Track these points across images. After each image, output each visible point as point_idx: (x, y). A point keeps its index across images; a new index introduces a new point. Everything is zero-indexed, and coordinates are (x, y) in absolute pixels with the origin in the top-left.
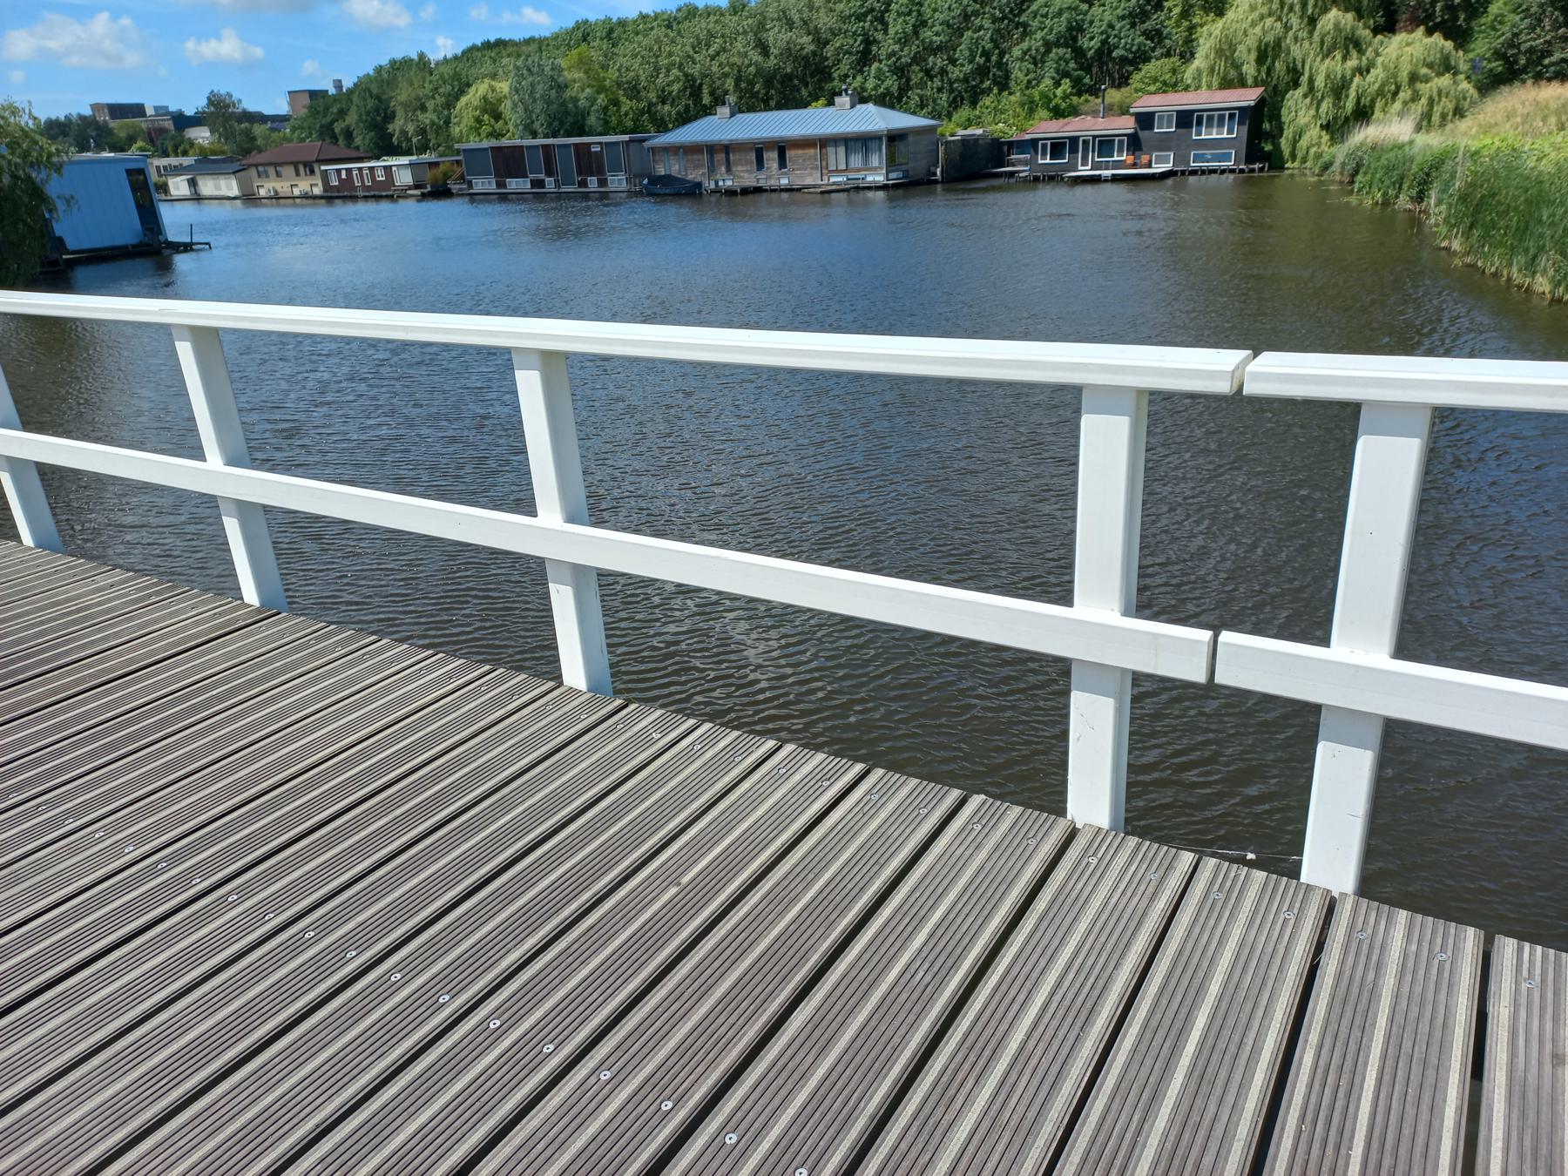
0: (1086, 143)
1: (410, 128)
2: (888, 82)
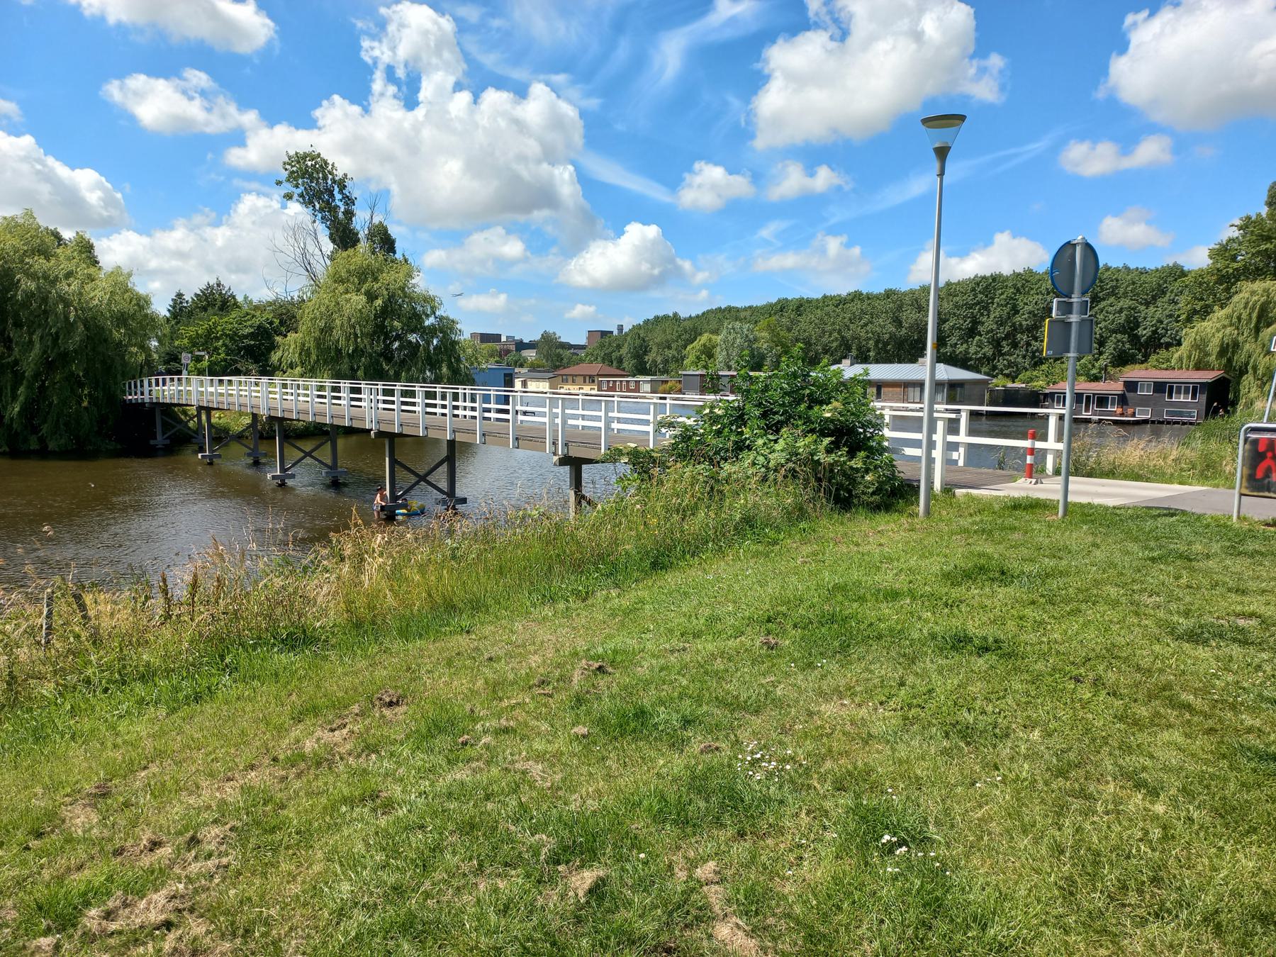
0: (1088, 398)
1: (659, 359)
2: (986, 349)
